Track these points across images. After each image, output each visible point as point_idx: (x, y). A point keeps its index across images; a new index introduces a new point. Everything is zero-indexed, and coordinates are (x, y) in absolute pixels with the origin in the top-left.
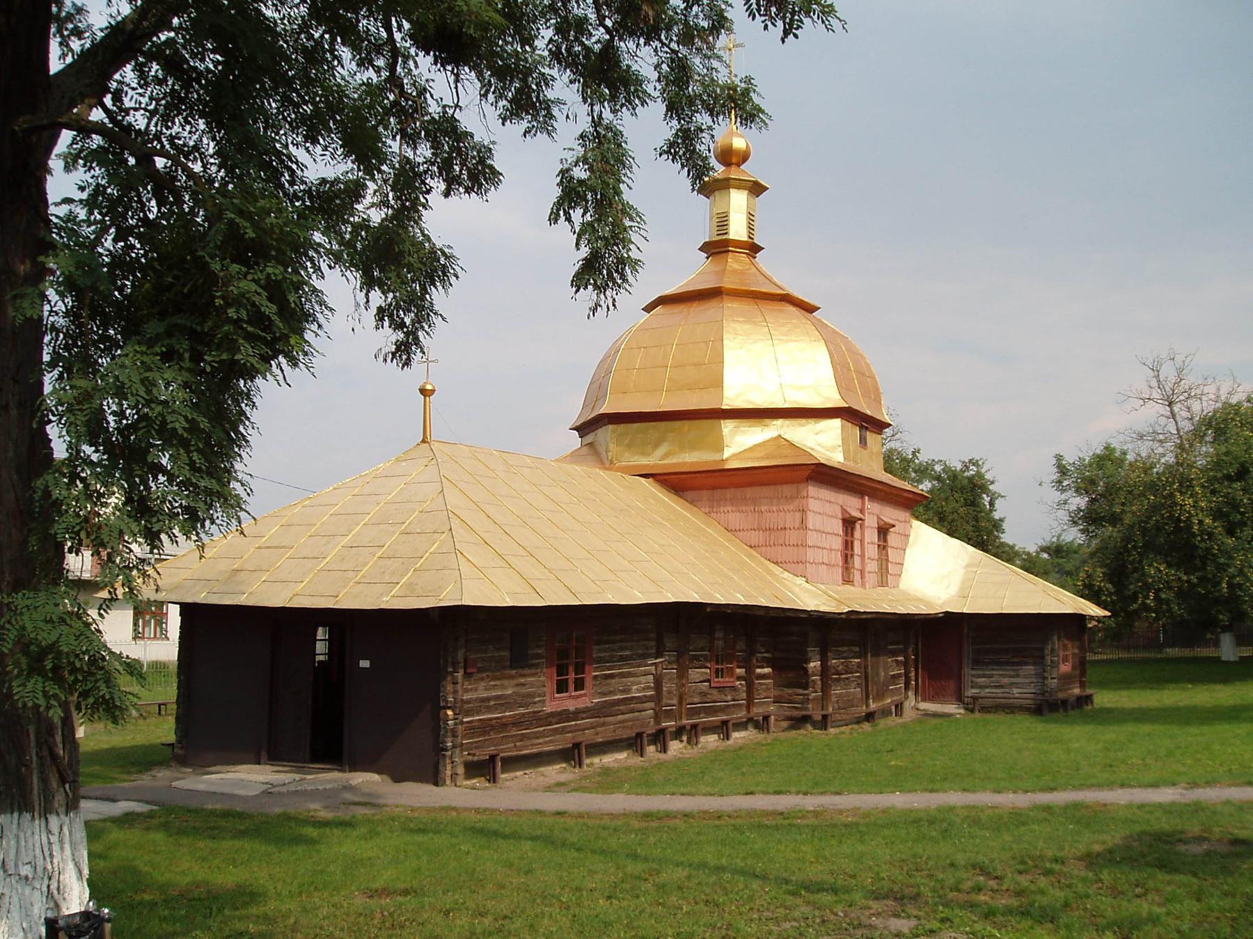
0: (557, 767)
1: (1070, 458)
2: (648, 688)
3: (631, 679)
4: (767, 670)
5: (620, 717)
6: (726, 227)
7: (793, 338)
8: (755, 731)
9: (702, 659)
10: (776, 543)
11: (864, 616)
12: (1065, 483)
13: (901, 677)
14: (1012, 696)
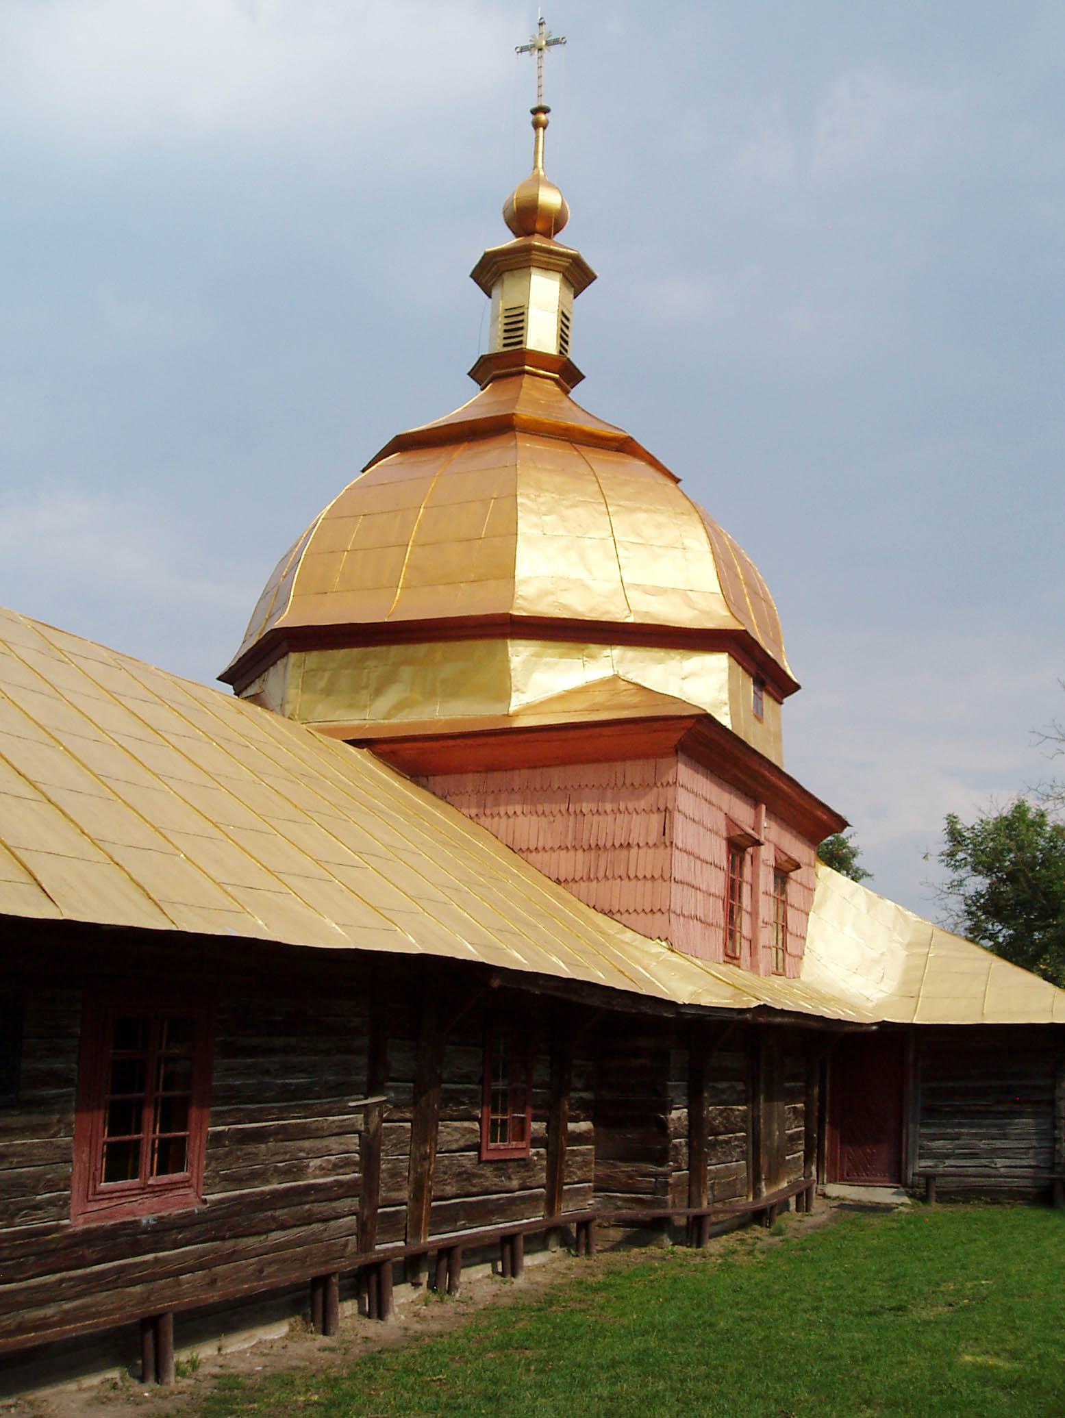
0: (93, 1381)
1: (968, 820)
2: (347, 1163)
3: (307, 1144)
4: (585, 1126)
5: (277, 1236)
6: (519, 333)
7: (644, 507)
8: (560, 1251)
9: (466, 1100)
10: (609, 874)
11: (778, 1020)
12: (961, 855)
13: (800, 1139)
14: (993, 1172)
